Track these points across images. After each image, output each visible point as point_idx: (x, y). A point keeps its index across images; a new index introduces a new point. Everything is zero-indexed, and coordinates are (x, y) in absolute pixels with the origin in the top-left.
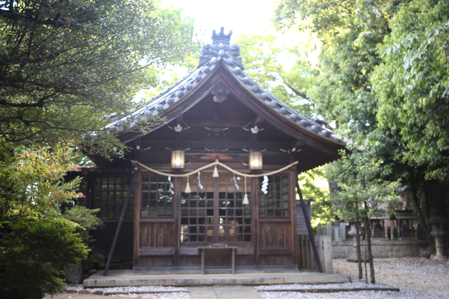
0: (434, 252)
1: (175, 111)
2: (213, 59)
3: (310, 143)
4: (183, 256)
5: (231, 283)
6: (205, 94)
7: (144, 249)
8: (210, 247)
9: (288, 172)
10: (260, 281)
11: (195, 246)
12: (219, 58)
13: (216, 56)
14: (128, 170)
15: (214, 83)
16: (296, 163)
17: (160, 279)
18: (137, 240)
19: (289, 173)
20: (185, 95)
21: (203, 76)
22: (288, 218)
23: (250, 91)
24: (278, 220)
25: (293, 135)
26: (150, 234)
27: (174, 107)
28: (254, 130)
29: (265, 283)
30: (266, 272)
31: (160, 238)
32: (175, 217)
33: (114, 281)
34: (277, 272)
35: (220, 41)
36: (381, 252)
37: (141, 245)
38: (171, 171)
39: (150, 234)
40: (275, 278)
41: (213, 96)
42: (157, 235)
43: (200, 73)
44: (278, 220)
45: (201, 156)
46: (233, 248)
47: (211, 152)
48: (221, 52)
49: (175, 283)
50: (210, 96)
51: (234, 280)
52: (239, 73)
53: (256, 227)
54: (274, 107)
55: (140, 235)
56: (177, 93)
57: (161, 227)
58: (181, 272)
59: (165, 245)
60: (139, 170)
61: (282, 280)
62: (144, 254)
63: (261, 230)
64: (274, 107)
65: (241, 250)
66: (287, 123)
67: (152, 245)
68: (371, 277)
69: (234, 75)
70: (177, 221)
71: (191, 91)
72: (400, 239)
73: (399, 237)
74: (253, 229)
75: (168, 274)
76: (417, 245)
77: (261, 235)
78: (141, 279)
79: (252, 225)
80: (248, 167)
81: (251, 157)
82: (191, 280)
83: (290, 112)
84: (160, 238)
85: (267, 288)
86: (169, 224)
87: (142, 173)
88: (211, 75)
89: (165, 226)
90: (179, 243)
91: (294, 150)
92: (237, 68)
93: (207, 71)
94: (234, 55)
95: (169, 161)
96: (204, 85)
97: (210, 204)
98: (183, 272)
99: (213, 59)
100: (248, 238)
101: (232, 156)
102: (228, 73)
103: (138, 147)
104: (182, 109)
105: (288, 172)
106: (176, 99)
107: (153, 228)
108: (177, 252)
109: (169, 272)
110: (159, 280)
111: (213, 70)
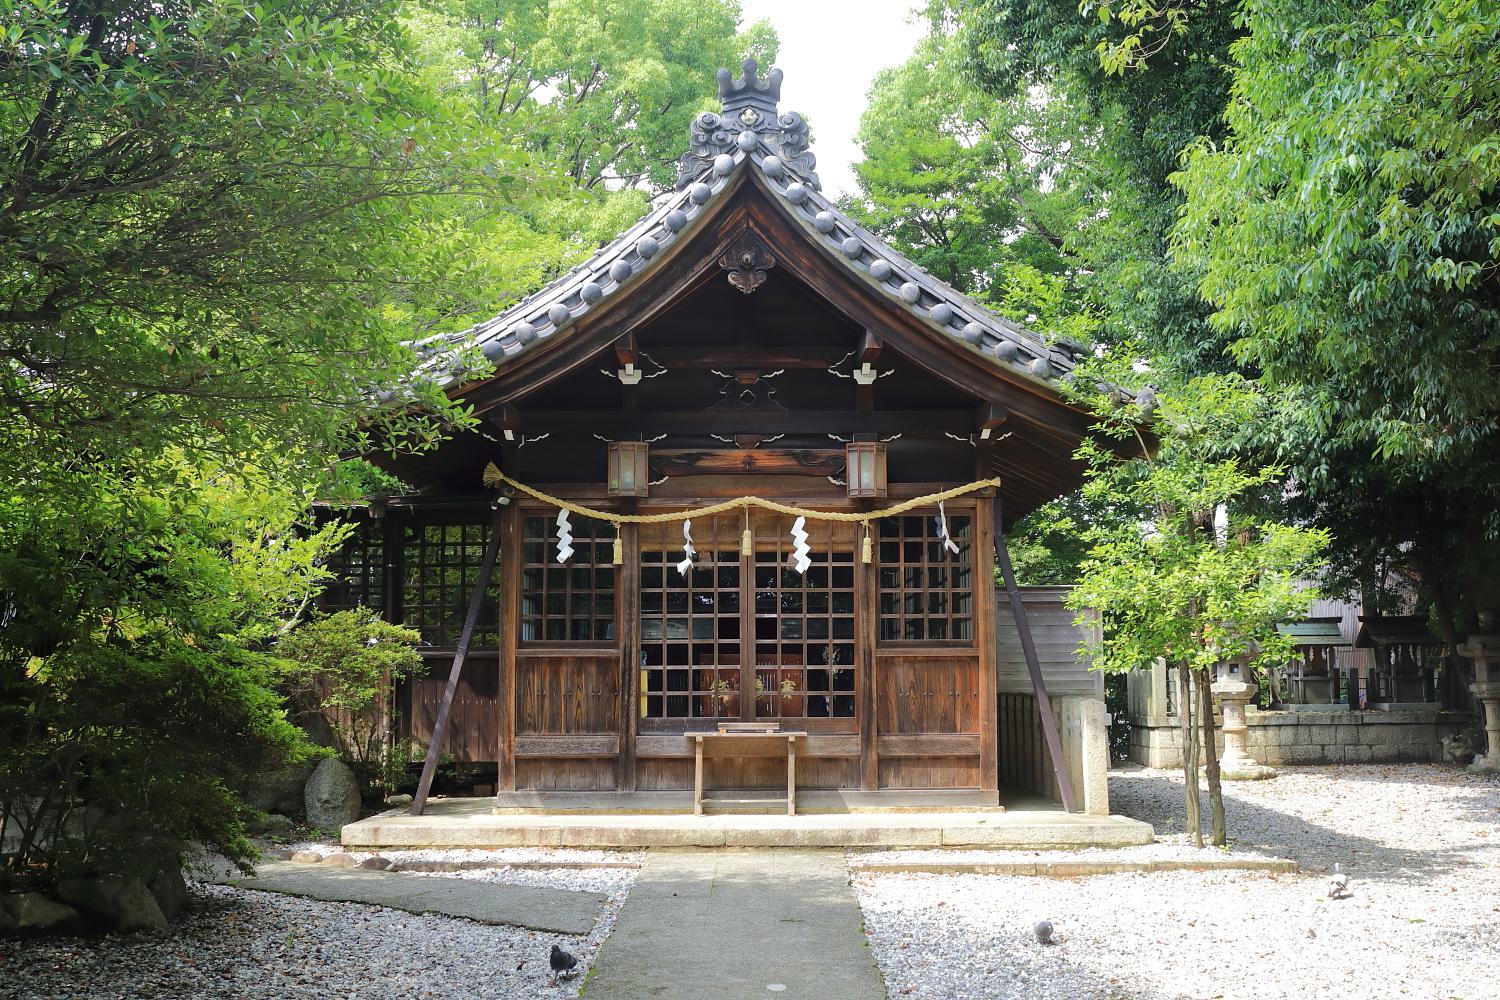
0: (1482, 746)
1: (608, 323)
2: (722, 160)
3: (1025, 413)
4: (643, 761)
5: (777, 841)
6: (701, 268)
7: (530, 737)
8: (723, 733)
9: (970, 502)
10: (868, 838)
11: (680, 728)
12: (739, 157)
13: (731, 150)
14: (1482, 617)
15: (727, 235)
16: (996, 482)
17: (562, 826)
18: (508, 711)
19: (974, 508)
20: (635, 271)
21: (691, 214)
22: (969, 645)
23: (836, 255)
24: (935, 652)
25: (974, 389)
26: (547, 692)
27: (603, 310)
28: (865, 376)
29: (883, 843)
30: (900, 810)
31: (579, 705)
32: (622, 645)
33: (427, 832)
34: (934, 810)
35: (747, 103)
36: (1323, 746)
37: (522, 726)
38: (608, 504)
39: (547, 692)
40: (913, 830)
41: (726, 273)
42: (569, 697)
43: (686, 203)
44: (935, 652)
45: (699, 457)
46: (792, 736)
47: (732, 446)
48: (744, 138)
49: (609, 841)
50: (717, 274)
51: (788, 834)
52: (804, 202)
53: (868, 675)
54: (911, 304)
55: (518, 698)
56: (614, 267)
57: (579, 674)
58: (639, 805)
59: (594, 728)
60: (513, 501)
61: (936, 834)
62: (529, 754)
63: (884, 682)
64: (911, 304)
65: (818, 745)
66: (956, 353)
67: (554, 727)
68: (1055, 866)
69: (788, 207)
70: (628, 655)
71: (654, 259)
72: (1386, 706)
73: (1384, 700)
74: (860, 678)
75: (600, 813)
76: (1436, 724)
77: (884, 698)
78: (509, 826)
79: (857, 666)
80: (843, 490)
81: (852, 460)
82: (656, 832)
83: (965, 317)
84: (579, 705)
85: (890, 858)
86: (604, 663)
87: (524, 510)
88: (718, 208)
89: (593, 669)
90: (633, 722)
91: (986, 434)
92: (795, 186)
93: (701, 200)
94: (787, 144)
95: (599, 474)
96: (698, 243)
97: (729, 602)
98: (646, 805)
99: (722, 160)
100: (844, 707)
101: (795, 456)
102: (767, 202)
103: (509, 435)
104: (631, 317)
105: (970, 502)
106: (610, 288)
107: (556, 674)
108: (627, 748)
109: (603, 807)
110: (562, 831)
111: (722, 193)
